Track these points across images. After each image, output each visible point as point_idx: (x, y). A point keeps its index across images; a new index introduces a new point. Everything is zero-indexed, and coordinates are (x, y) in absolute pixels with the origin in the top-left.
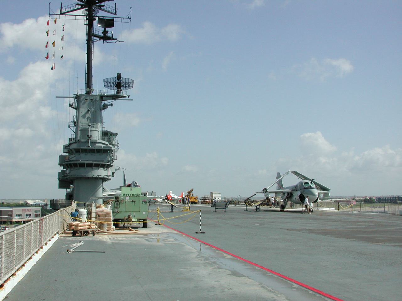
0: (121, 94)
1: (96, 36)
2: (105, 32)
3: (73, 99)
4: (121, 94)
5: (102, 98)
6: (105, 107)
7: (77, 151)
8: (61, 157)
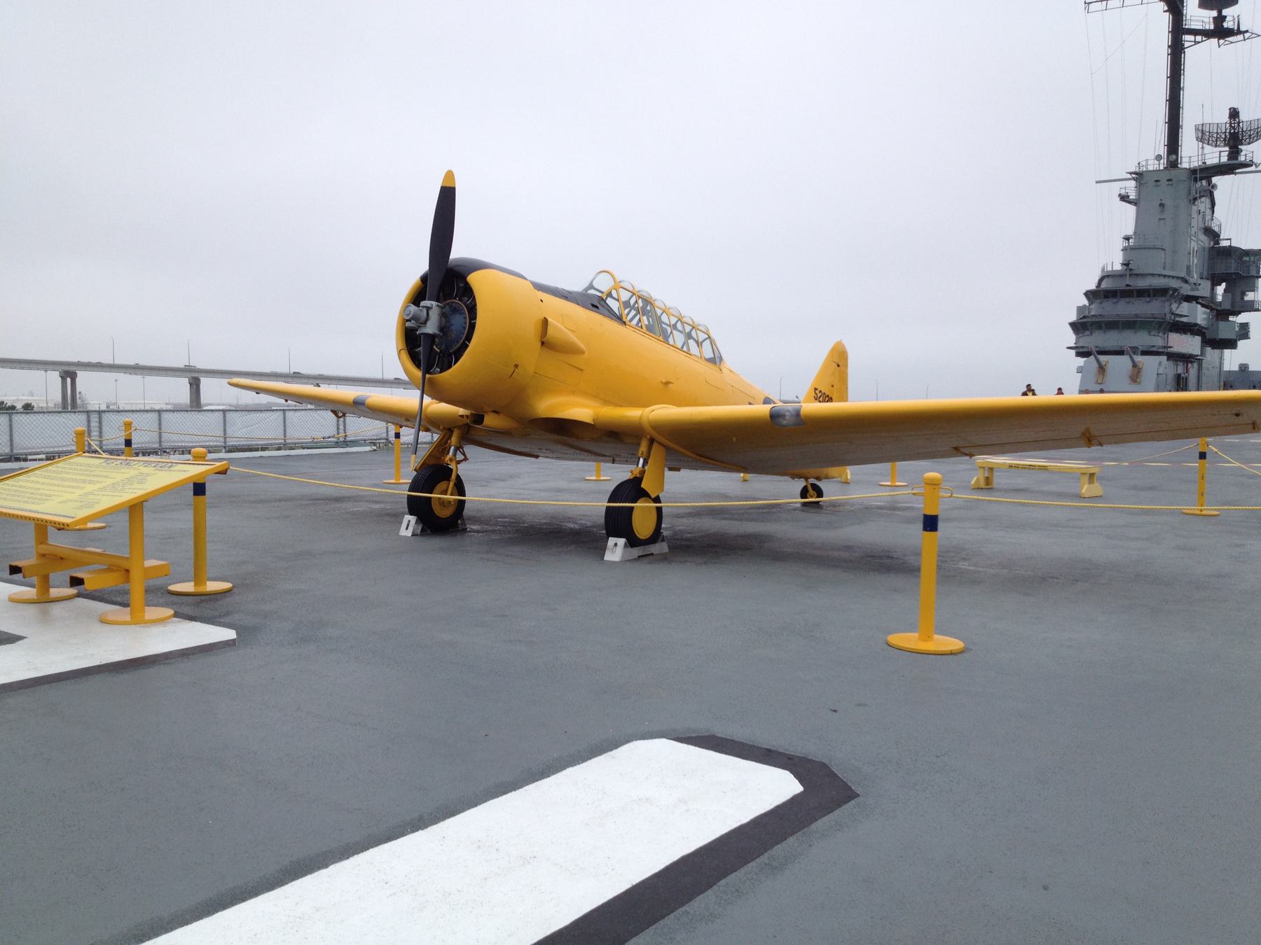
0: (1242, 158)
1: (1195, 32)
2: (1220, 19)
3: (1133, 183)
4: (1242, 158)
5: (1206, 173)
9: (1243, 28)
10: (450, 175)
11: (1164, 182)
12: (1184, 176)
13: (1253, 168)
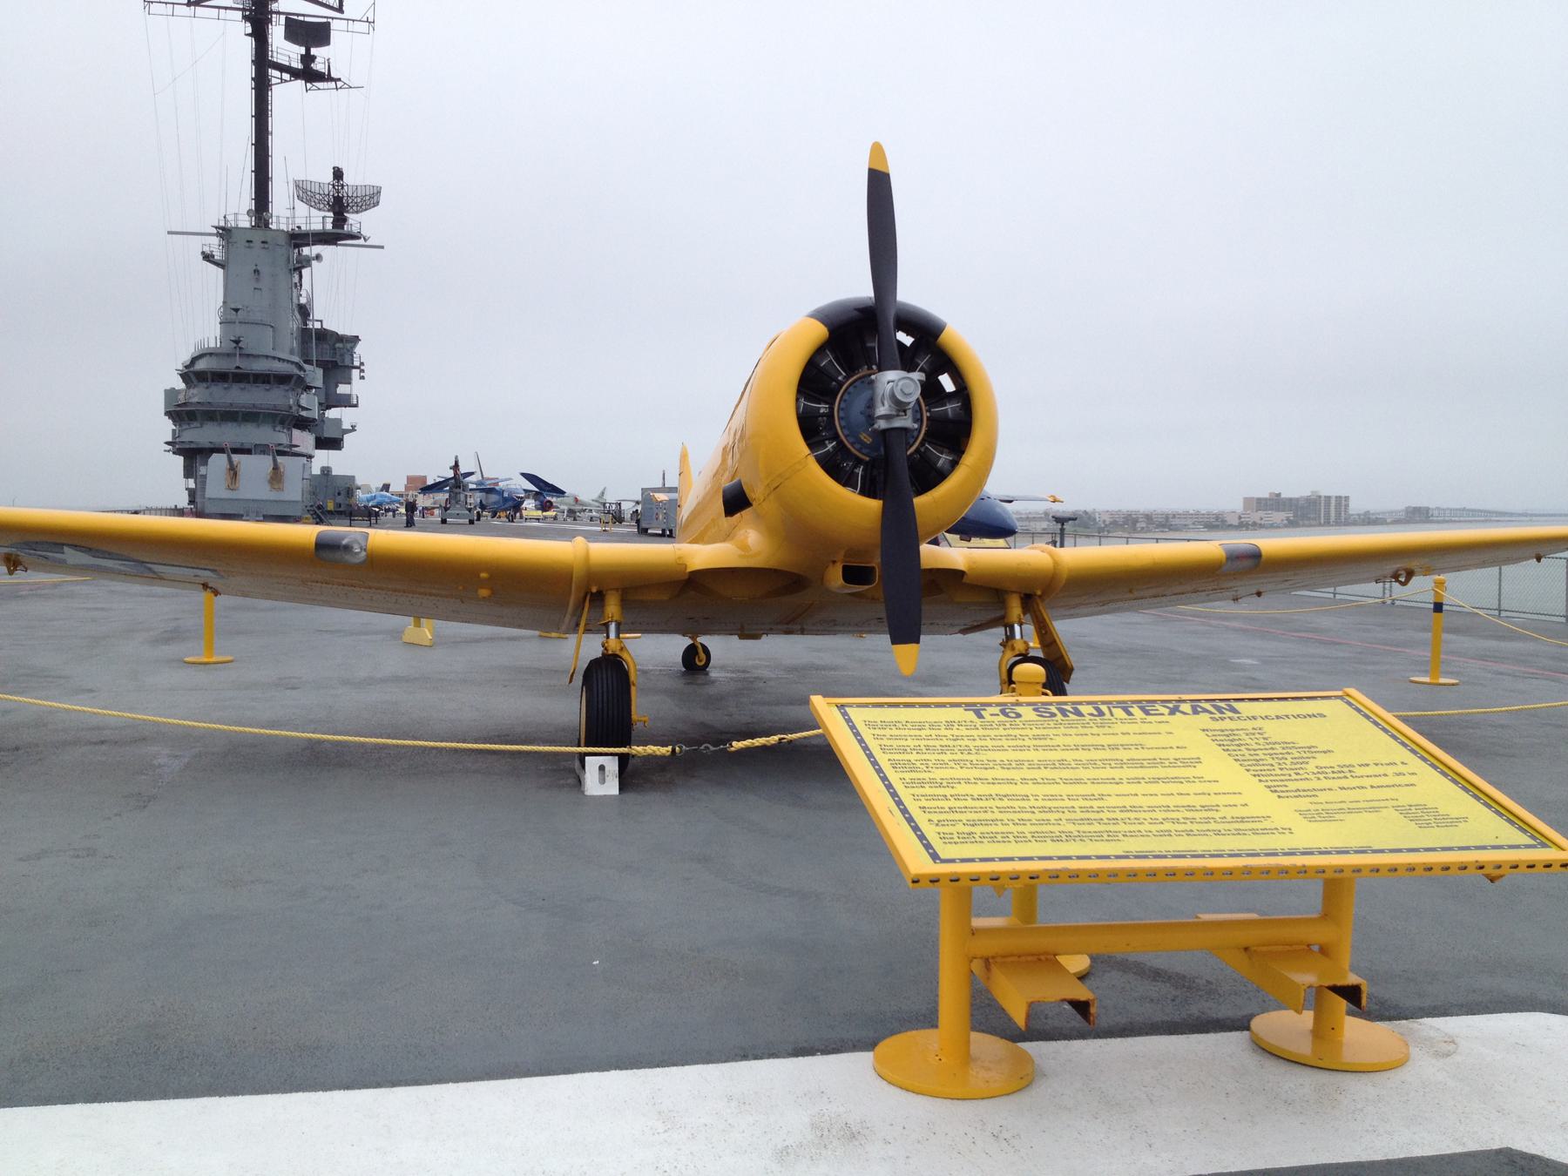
2: (308, 59)
3: (215, 240)
5: (299, 238)
6: (305, 262)
7: (220, 377)
8: (170, 394)
9: (333, 75)
10: (877, 150)
11: (257, 244)
12: (282, 240)
13: (361, 242)
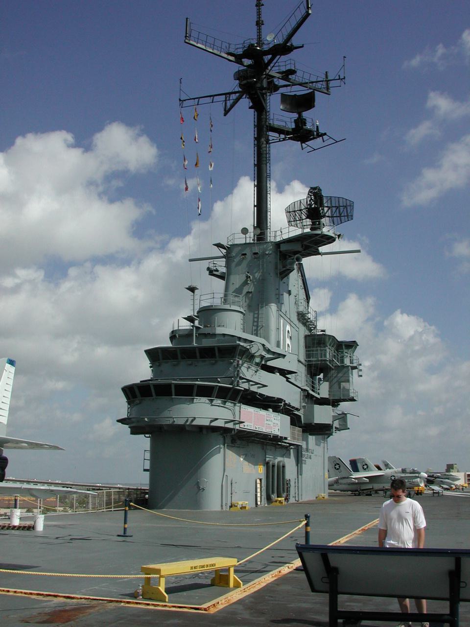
2: (300, 122)
